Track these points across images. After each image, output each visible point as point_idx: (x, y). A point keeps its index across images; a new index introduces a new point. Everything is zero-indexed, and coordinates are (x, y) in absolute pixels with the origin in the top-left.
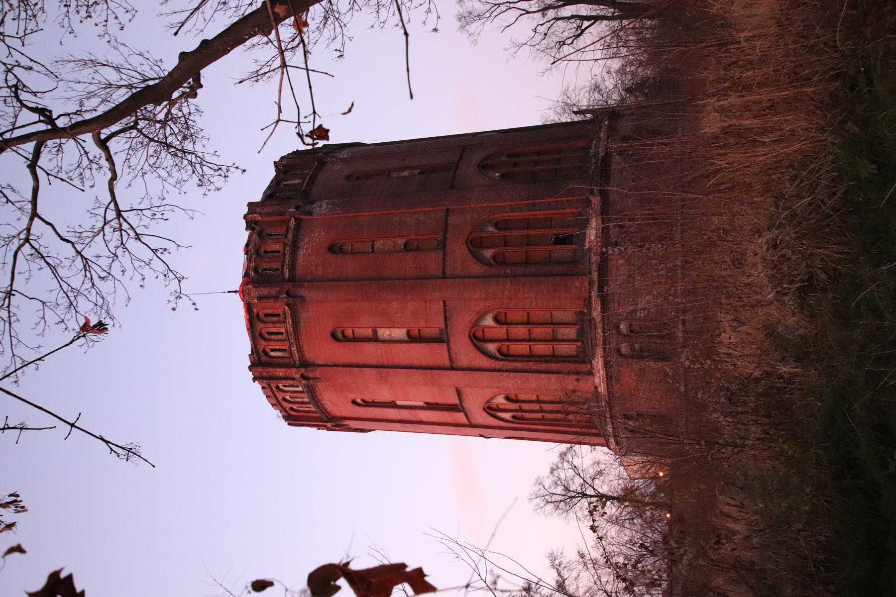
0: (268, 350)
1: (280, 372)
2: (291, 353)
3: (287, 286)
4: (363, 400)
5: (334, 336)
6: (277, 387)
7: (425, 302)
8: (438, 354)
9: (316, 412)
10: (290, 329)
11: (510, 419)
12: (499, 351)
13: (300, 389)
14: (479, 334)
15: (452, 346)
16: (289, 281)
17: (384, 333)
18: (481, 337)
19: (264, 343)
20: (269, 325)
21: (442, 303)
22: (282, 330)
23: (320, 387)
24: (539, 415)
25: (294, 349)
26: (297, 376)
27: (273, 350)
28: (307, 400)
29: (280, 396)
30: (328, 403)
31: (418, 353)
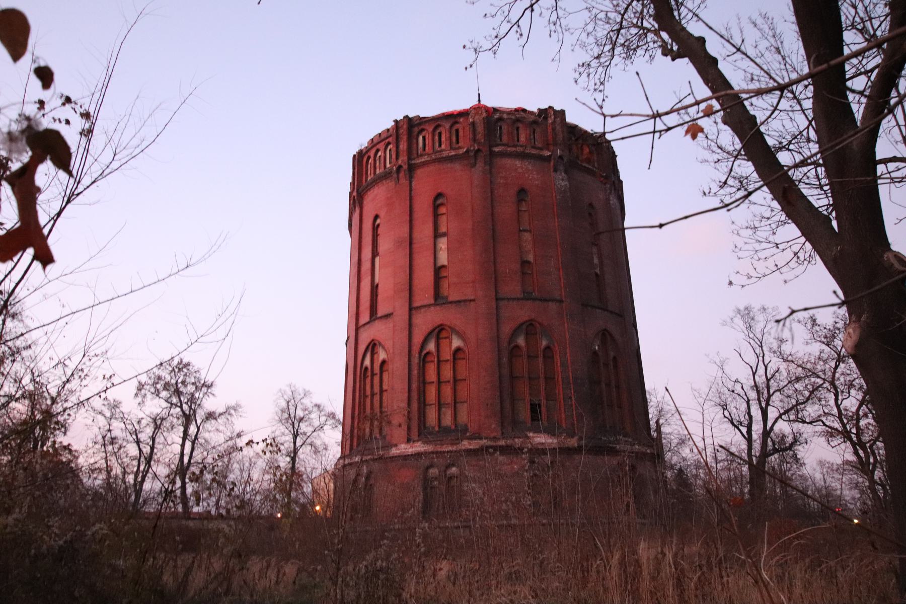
0: (424, 133)
1: (403, 146)
2: (422, 155)
7: (473, 282)
8: (424, 296)
10: (445, 154)
17: (443, 243)
19: (431, 129)
21: (472, 298)
22: (443, 147)
25: (426, 158)
26: (400, 162)
27: (424, 138)
28: (378, 172)
29: (381, 146)
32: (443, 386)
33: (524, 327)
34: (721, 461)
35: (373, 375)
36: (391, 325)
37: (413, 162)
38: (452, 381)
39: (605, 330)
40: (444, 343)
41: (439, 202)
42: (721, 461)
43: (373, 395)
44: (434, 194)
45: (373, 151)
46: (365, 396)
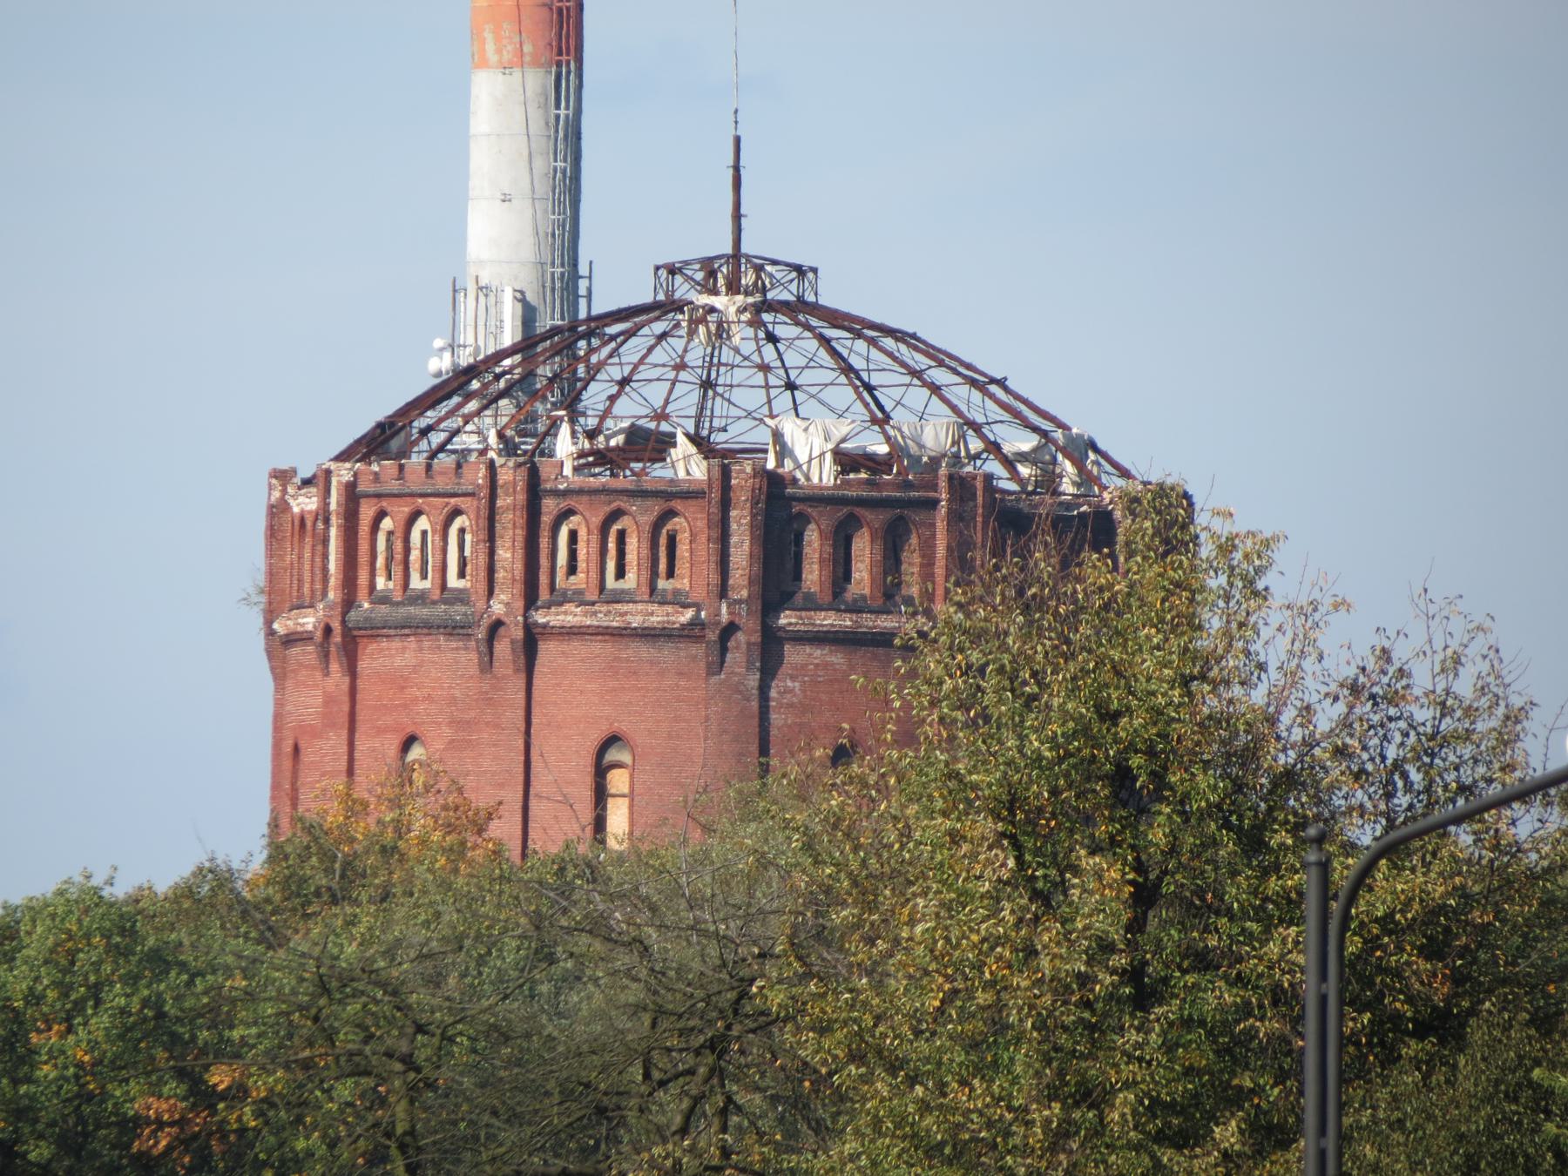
1: (509, 555)
5: (612, 740)
22: (631, 580)
26: (497, 608)
27: (573, 536)
37: (540, 617)
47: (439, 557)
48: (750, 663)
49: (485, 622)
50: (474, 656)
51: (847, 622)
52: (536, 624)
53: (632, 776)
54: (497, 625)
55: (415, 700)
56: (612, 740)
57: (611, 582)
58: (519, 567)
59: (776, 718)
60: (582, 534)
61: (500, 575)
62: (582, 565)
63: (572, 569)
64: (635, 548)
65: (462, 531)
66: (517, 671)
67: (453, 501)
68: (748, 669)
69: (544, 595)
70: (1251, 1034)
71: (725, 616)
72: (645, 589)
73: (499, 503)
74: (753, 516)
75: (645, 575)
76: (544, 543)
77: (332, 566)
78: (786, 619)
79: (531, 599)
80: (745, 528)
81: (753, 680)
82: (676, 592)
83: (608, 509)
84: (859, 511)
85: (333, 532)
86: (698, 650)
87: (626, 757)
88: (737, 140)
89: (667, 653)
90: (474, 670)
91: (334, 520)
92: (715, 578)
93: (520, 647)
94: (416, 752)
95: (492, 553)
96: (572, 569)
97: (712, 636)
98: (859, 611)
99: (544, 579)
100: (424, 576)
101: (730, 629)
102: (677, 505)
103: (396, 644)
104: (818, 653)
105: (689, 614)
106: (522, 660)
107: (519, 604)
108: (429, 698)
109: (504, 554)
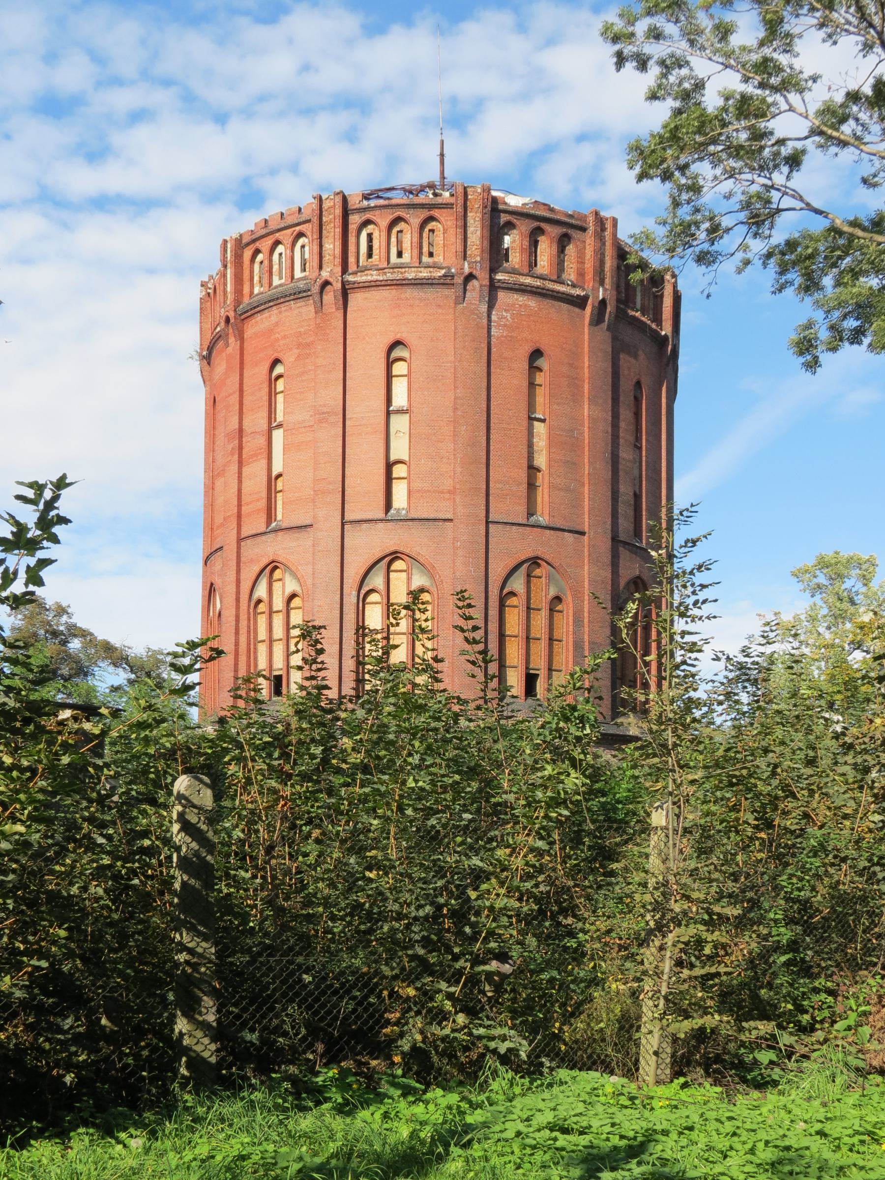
0: (370, 228)
1: (332, 246)
2: (366, 269)
3: (483, 275)
4: (279, 376)
5: (397, 343)
6: (301, 235)
7: (452, 492)
8: (365, 501)
9: (252, 293)
10: (411, 275)
11: (255, 596)
12: (259, 601)
13: (298, 274)
14: (277, 574)
15: (381, 525)
16: (491, 280)
17: (399, 423)
18: (392, 568)
19: (384, 223)
20: (416, 236)
21: (449, 516)
22: (406, 258)
23: (304, 310)
24: (262, 634)
25: (374, 276)
26: (325, 274)
27: (370, 237)
28: (276, 281)
29: (286, 236)
30: (274, 319)
31: (508, 474)
32: (275, 616)
33: (525, 566)
34: (294, 627)
35: (271, 612)
36: (310, 543)
37: (351, 278)
38: (267, 612)
39: (638, 577)
40: (277, 586)
41: (395, 354)
42: (294, 627)
43: (271, 641)
44: (390, 339)
45: (269, 241)
46: (257, 642)
47: (289, 261)
48: (481, 296)
49: (319, 282)
50: (312, 308)
51: (538, 283)
52: (349, 282)
53: (409, 467)
54: (326, 283)
55: (277, 340)
56: (397, 343)
57: (394, 259)
58: (338, 251)
59: (494, 331)
60: (376, 235)
61: (327, 258)
62: (376, 251)
63: (370, 255)
64: (408, 240)
65: (303, 247)
66: (337, 309)
67: (297, 228)
68: (480, 301)
69: (352, 267)
70: (275, 1041)
71: (467, 270)
72: (416, 260)
73: (324, 219)
74: (484, 214)
75: (416, 252)
76: (352, 240)
77: (229, 289)
78: (499, 276)
79: (345, 270)
80: (478, 224)
81: (484, 308)
82: (434, 263)
83: (391, 217)
84: (543, 225)
85: (229, 271)
86: (450, 293)
87: (405, 354)
88: (442, 142)
89: (430, 293)
90: (312, 314)
91: (229, 265)
92: (460, 248)
93: (339, 293)
94: (279, 369)
95: (321, 246)
96: (370, 255)
97: (459, 280)
98: (545, 279)
99: (352, 259)
100: (281, 278)
101: (470, 277)
102: (435, 213)
103: (266, 314)
104: (521, 299)
105: (443, 272)
106: (341, 302)
107: (339, 270)
108: (285, 337)
109: (328, 246)
